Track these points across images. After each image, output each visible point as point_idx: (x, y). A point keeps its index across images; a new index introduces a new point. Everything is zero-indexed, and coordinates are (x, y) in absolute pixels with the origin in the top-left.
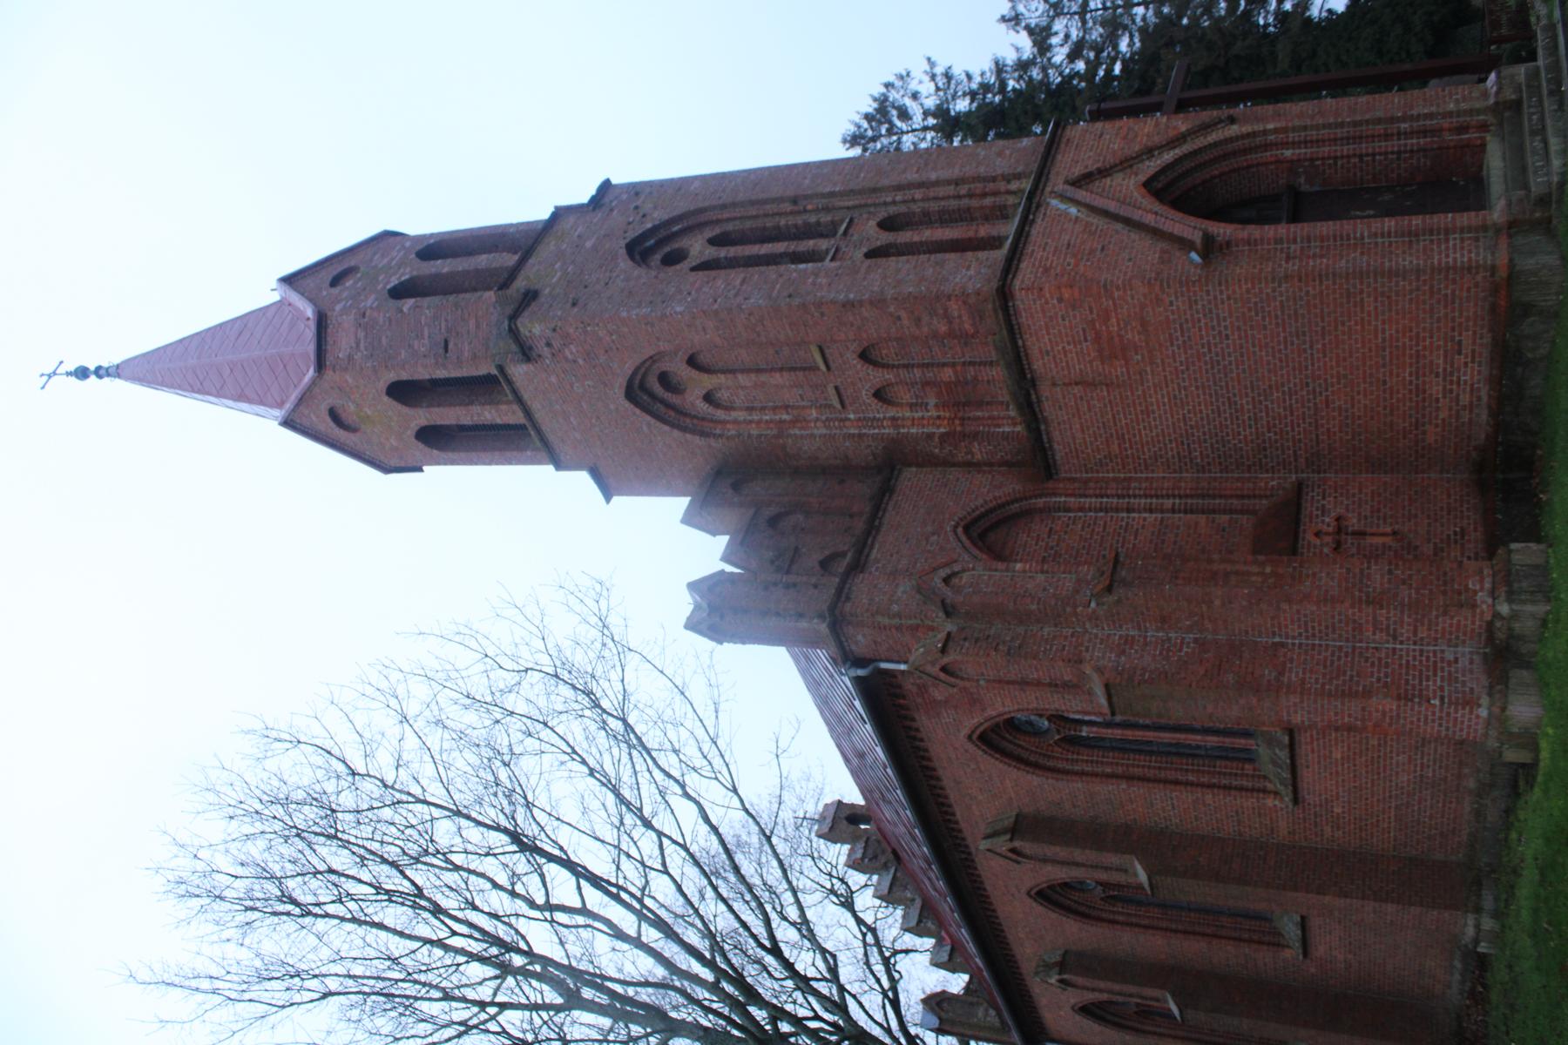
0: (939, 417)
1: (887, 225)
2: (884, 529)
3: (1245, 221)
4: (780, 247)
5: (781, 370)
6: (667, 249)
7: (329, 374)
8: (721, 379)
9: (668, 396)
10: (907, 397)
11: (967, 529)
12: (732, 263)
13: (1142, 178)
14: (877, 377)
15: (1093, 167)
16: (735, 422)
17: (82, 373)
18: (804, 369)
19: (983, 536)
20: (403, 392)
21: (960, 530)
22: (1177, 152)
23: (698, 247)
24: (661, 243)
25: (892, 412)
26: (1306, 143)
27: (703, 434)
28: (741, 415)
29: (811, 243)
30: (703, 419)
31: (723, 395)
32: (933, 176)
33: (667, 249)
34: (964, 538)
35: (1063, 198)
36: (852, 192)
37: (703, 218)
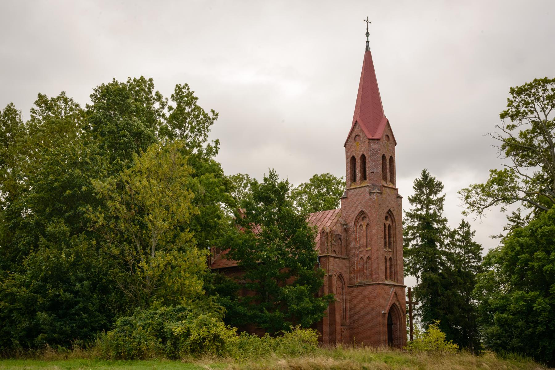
1: (390, 258)
3: (388, 317)
4: (387, 240)
7: (367, 141)
8: (365, 229)
9: (361, 217)
12: (385, 230)
13: (395, 302)
14: (365, 259)
15: (398, 295)
17: (368, 34)
20: (363, 157)
22: (399, 307)
23: (389, 222)
24: (390, 215)
25: (359, 260)
26: (400, 326)
32: (398, 266)
35: (393, 290)
36: (396, 252)
37: (394, 222)
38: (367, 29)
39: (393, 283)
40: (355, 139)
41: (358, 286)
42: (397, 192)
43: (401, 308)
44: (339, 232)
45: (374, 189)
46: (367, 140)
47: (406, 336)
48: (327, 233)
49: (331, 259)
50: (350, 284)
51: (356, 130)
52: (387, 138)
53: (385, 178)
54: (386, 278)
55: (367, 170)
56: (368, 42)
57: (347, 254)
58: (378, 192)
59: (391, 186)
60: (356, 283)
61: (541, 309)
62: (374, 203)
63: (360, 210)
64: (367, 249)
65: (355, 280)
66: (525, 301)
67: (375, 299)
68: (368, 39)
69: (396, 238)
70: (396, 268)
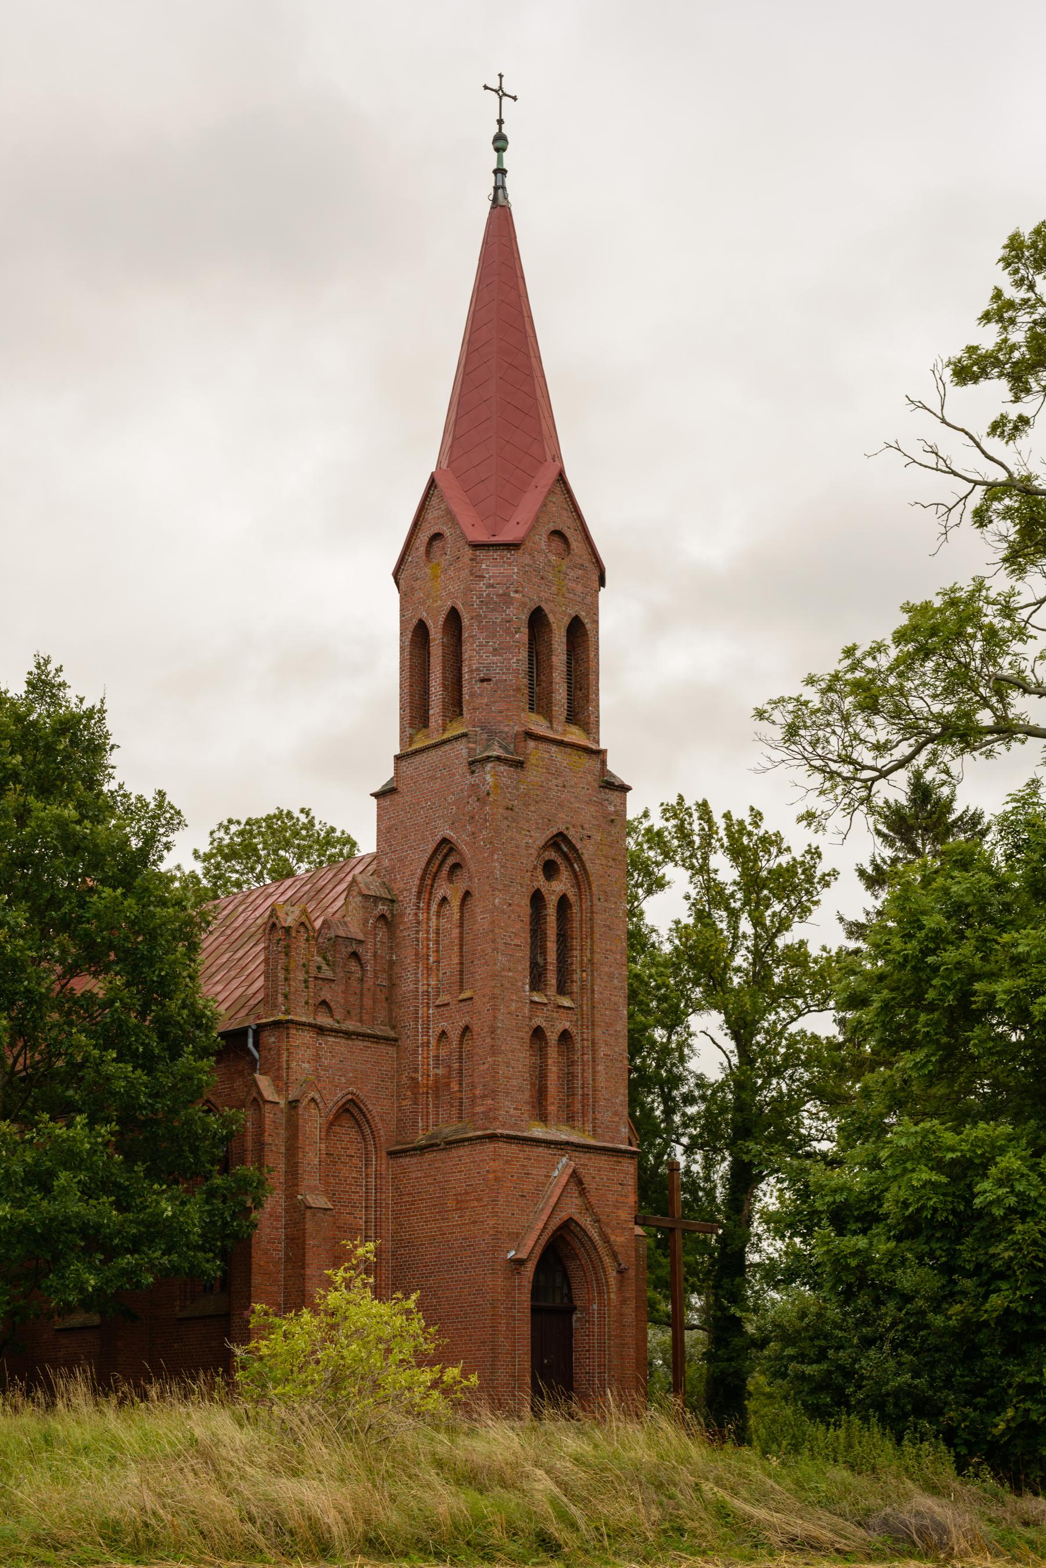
0: (428, 1076)
1: (565, 1036)
2: (349, 1042)
5: (461, 964)
6: (559, 861)
7: (468, 552)
8: (457, 916)
9: (446, 868)
10: (442, 1053)
11: (352, 1100)
14: (454, 1035)
16: (428, 919)
17: (500, 143)
18: (461, 981)
19: (347, 1110)
20: (454, 618)
21: (350, 1096)
27: (420, 893)
28: (433, 923)
29: (554, 982)
30: (431, 893)
31: (446, 910)
33: (559, 861)
34: (344, 1100)
35: (567, 1165)
38: (500, 122)
39: (575, 1138)
40: (428, 552)
41: (423, 1149)
42: (604, 763)
43: (606, 1241)
44: (355, 930)
45: (487, 747)
46: (467, 548)
47: (1029, 1384)
48: (287, 930)
49: (302, 1038)
50: (398, 1143)
51: (431, 515)
52: (557, 544)
53: (539, 702)
54: (543, 1118)
55: (465, 669)
56: (500, 171)
57: (390, 1018)
58: (498, 759)
59: (575, 735)
60: (421, 1139)
61: (1012, 1200)
62: (485, 803)
63: (439, 838)
64: (462, 996)
65: (415, 1123)
66: (939, 1166)
67: (479, 1200)
68: (500, 160)
69: (592, 952)
70: (589, 1075)
